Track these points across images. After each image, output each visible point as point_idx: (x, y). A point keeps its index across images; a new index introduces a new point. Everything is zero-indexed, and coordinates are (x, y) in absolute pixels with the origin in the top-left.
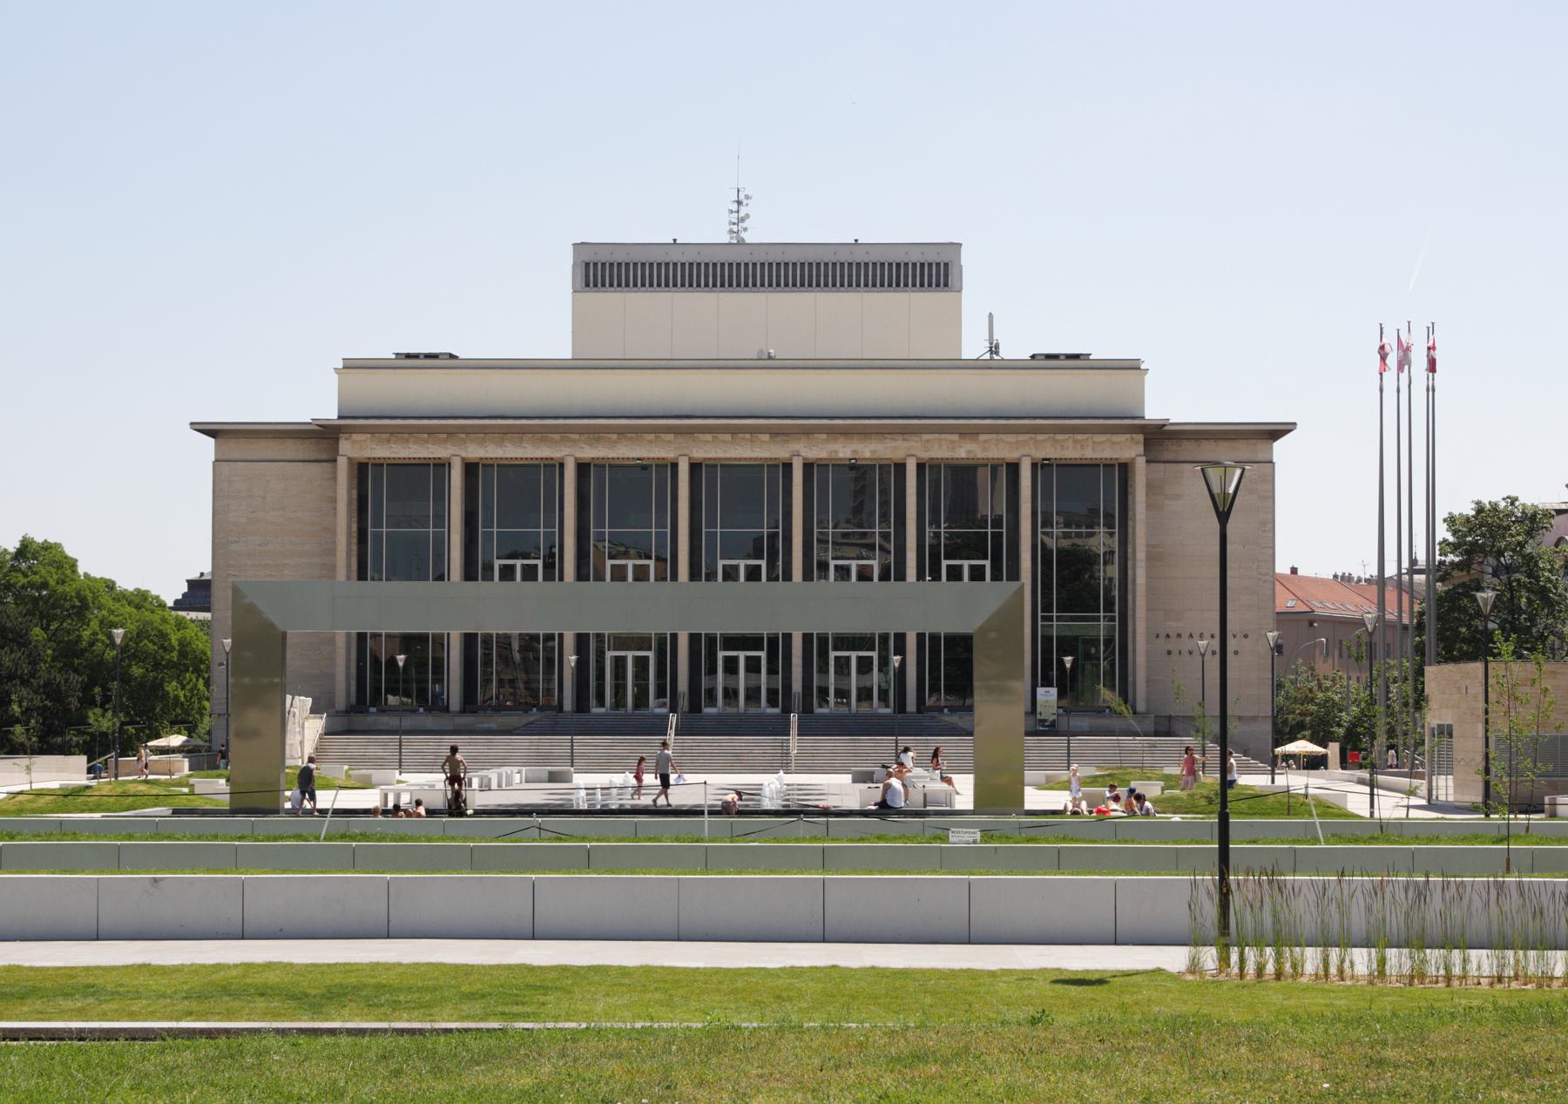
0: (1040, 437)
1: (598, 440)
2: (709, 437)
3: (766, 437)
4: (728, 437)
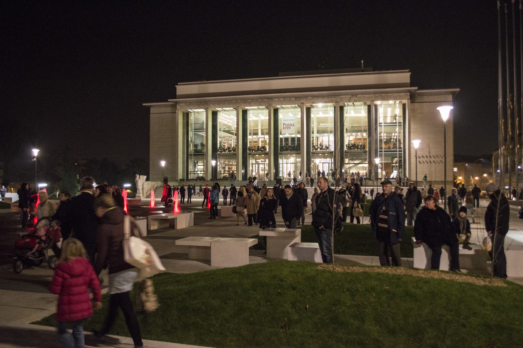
0: (377, 95)
1: (246, 102)
2: (277, 99)
3: (293, 99)
4: (283, 99)
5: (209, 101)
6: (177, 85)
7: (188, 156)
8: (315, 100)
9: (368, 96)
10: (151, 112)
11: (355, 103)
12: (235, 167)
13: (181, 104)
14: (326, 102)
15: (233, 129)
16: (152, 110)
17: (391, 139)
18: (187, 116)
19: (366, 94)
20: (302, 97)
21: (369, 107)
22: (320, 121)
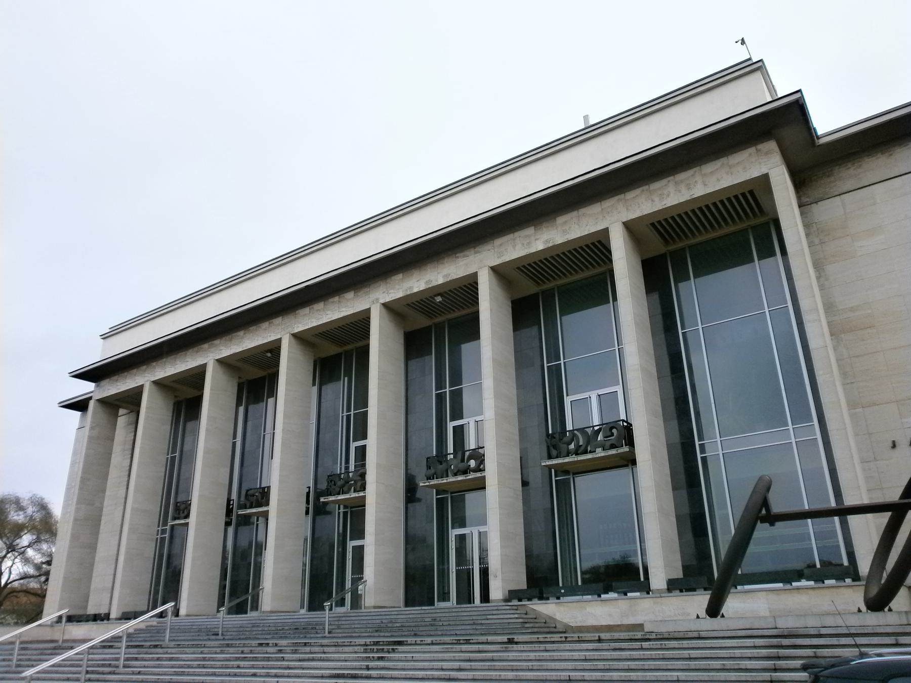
1: (231, 340)
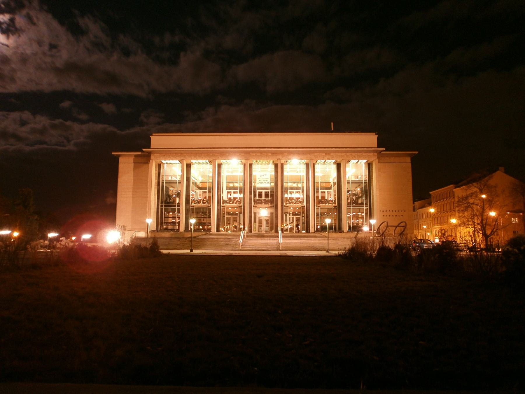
0: (348, 154)
1: (223, 155)
2: (254, 154)
4: (260, 154)
5: (216, 152)
6: (152, 135)
7: (165, 217)
8: (290, 157)
9: (340, 154)
10: (120, 161)
11: (327, 161)
12: (190, 236)
13: (155, 155)
14: (301, 159)
15: (331, 180)
16: (121, 160)
17: (173, 211)
18: (159, 166)
19: (252, 153)
20: (212, 154)
21: (276, 166)
22: (231, 179)
